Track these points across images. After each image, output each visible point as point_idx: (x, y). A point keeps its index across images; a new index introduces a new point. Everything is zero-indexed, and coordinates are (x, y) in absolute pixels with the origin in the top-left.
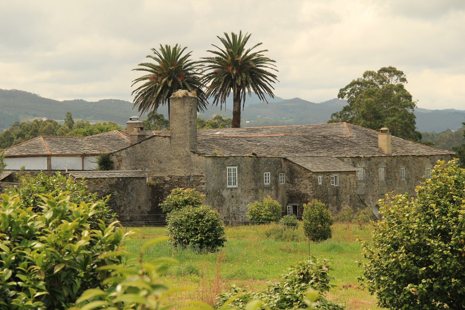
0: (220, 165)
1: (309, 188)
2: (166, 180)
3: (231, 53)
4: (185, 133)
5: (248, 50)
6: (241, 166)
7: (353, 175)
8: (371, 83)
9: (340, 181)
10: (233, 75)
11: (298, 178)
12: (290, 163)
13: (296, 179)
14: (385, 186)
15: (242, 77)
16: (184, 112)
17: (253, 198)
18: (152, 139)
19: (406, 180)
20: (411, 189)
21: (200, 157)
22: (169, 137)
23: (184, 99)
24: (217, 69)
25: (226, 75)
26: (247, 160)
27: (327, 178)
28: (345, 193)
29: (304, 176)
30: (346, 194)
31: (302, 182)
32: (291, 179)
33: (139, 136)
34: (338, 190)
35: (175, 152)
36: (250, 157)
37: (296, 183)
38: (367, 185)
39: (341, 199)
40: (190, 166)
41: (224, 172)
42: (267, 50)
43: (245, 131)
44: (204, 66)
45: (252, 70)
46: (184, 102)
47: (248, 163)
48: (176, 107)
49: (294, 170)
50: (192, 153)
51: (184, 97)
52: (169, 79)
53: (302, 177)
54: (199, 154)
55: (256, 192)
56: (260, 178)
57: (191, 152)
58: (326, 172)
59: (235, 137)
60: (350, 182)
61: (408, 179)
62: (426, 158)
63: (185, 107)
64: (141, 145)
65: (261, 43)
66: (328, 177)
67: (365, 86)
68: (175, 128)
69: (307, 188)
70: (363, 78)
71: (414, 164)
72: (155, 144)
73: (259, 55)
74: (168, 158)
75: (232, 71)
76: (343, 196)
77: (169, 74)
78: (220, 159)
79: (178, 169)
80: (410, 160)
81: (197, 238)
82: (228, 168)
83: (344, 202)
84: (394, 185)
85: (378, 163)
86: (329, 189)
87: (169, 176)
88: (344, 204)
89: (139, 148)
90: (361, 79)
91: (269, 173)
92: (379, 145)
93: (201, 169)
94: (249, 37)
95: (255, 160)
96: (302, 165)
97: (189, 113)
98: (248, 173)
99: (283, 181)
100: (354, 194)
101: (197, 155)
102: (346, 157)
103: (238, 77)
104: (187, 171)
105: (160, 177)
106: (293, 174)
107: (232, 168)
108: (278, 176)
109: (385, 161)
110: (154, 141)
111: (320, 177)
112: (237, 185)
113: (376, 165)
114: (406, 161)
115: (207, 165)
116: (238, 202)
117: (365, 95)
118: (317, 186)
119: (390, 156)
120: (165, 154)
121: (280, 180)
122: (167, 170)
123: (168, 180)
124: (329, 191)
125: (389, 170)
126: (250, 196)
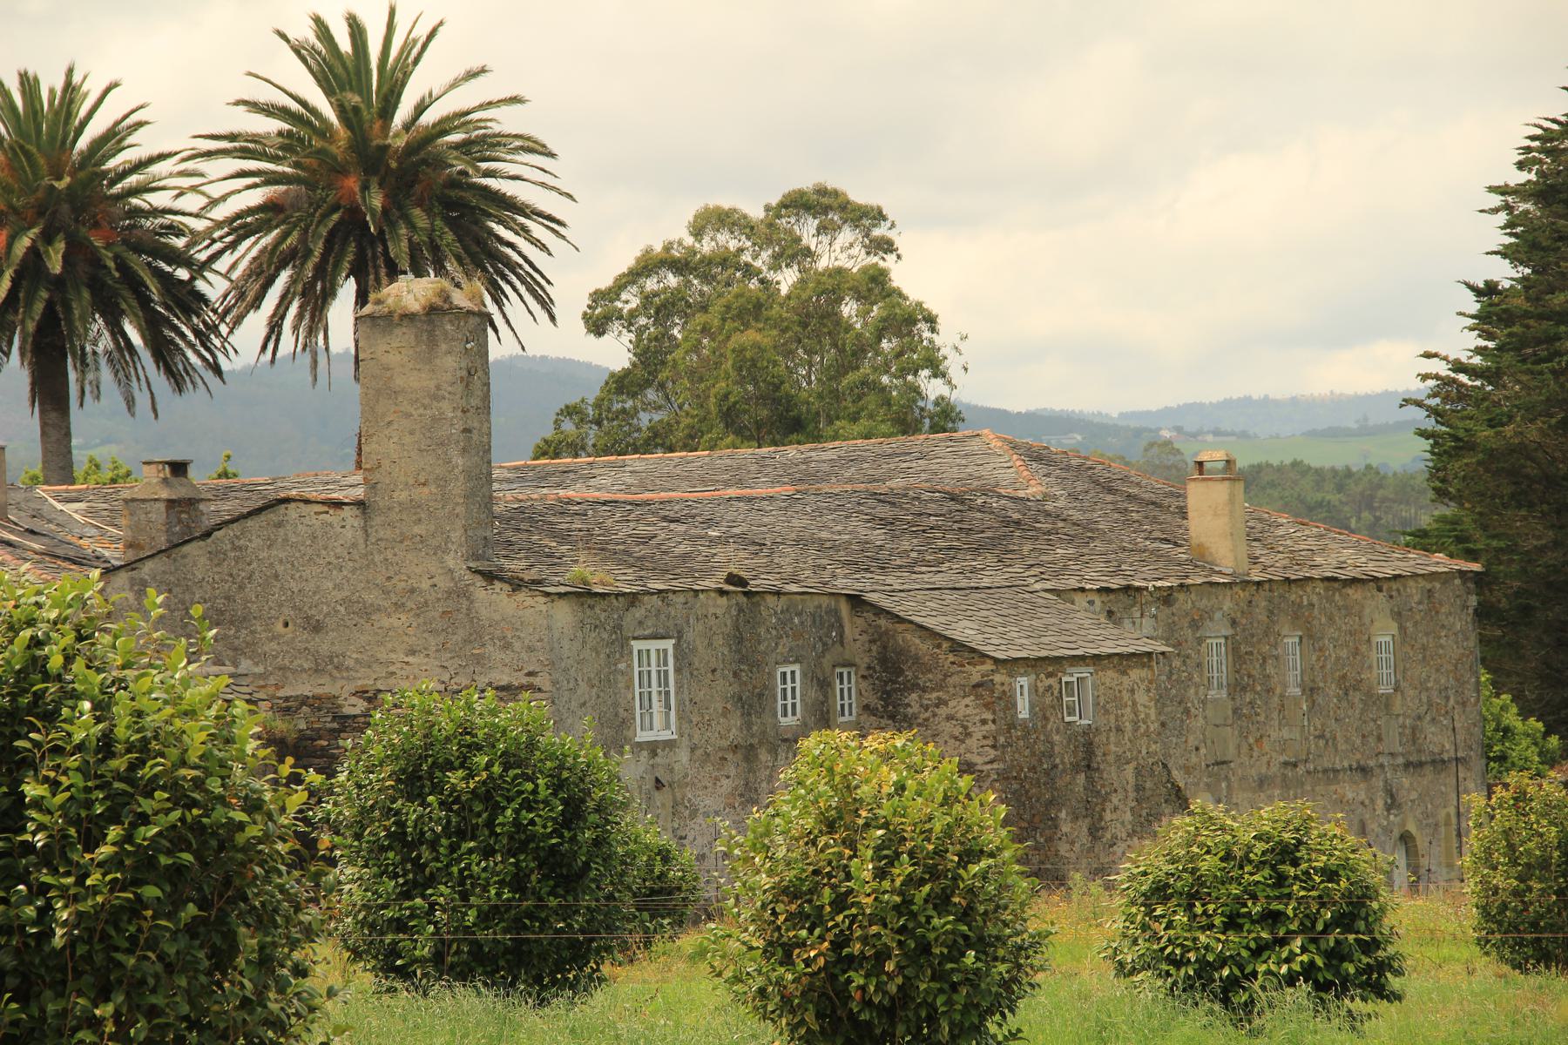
0: (605, 636)
1: (979, 735)
2: (348, 711)
3: (356, 109)
4: (442, 482)
5: (423, 100)
6: (689, 635)
7: (1144, 673)
8: (726, 260)
9: (1096, 704)
10: (373, 216)
11: (924, 690)
12: (883, 622)
13: (914, 696)
14: (1230, 722)
15: (412, 226)
16: (432, 384)
17: (736, 789)
18: (270, 516)
19: (1304, 691)
20: (1322, 736)
21: (521, 596)
22: (360, 504)
23: (430, 322)
24: (282, 188)
25: (336, 217)
26: (712, 610)
27: (1050, 687)
28: (1118, 758)
29: (951, 680)
30: (1121, 761)
31: (943, 711)
32: (889, 694)
33: (171, 503)
34: (1091, 744)
35: (389, 578)
36: (721, 592)
37: (915, 716)
38: (1162, 718)
39: (1103, 786)
40: (466, 641)
41: (622, 666)
42: (515, 100)
43: (509, 481)
44: (202, 175)
45: (453, 193)
46: (431, 334)
47: (712, 621)
48: (393, 359)
49: (901, 652)
50: (479, 577)
51: (432, 311)
52: (48, 237)
53: (940, 687)
54: (517, 585)
55: (747, 759)
56: (760, 695)
57: (477, 572)
58: (1046, 658)
59: (604, 503)
60: (1134, 704)
61: (1312, 690)
62: (1375, 592)
63: (438, 361)
64: (212, 548)
65: (483, 71)
66: (1052, 681)
67: (707, 278)
68: (386, 463)
69: (969, 735)
70: (689, 241)
71: (1331, 618)
72: (286, 540)
73: (477, 125)
74: (356, 607)
75: (364, 198)
76: (1110, 773)
77: (41, 214)
78: (604, 604)
79: (410, 659)
80: (1315, 599)
81: (1288, 961)
82: (637, 645)
83: (1115, 799)
84: (1262, 718)
85: (1201, 618)
86: (1056, 738)
87: (360, 693)
88: (1116, 809)
89: (203, 560)
90: (680, 243)
91: (797, 668)
92: (1193, 533)
93: (524, 655)
94: (432, 34)
95: (741, 610)
96: (938, 629)
97: (459, 388)
98: (714, 671)
99: (794, 705)
100: (1151, 761)
101: (507, 587)
102: (1083, 590)
103: (393, 225)
104: (452, 665)
105: (316, 698)
106: (900, 672)
107: (653, 645)
108: (829, 685)
109: (1227, 605)
110: (280, 525)
111: (1024, 681)
112: (673, 728)
113: (1195, 625)
114: (1300, 606)
115: (557, 635)
116: (680, 808)
117: (724, 320)
118: (1012, 726)
119: (1246, 583)
120: (337, 587)
121: (839, 702)
122: (350, 663)
123: (356, 711)
124: (1057, 749)
125: (1243, 649)
126: (725, 782)
